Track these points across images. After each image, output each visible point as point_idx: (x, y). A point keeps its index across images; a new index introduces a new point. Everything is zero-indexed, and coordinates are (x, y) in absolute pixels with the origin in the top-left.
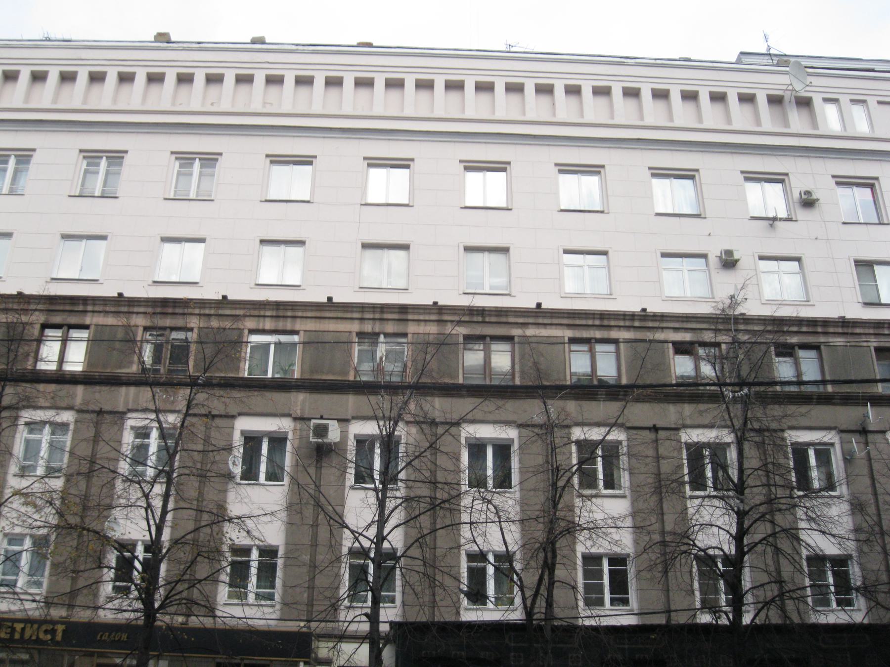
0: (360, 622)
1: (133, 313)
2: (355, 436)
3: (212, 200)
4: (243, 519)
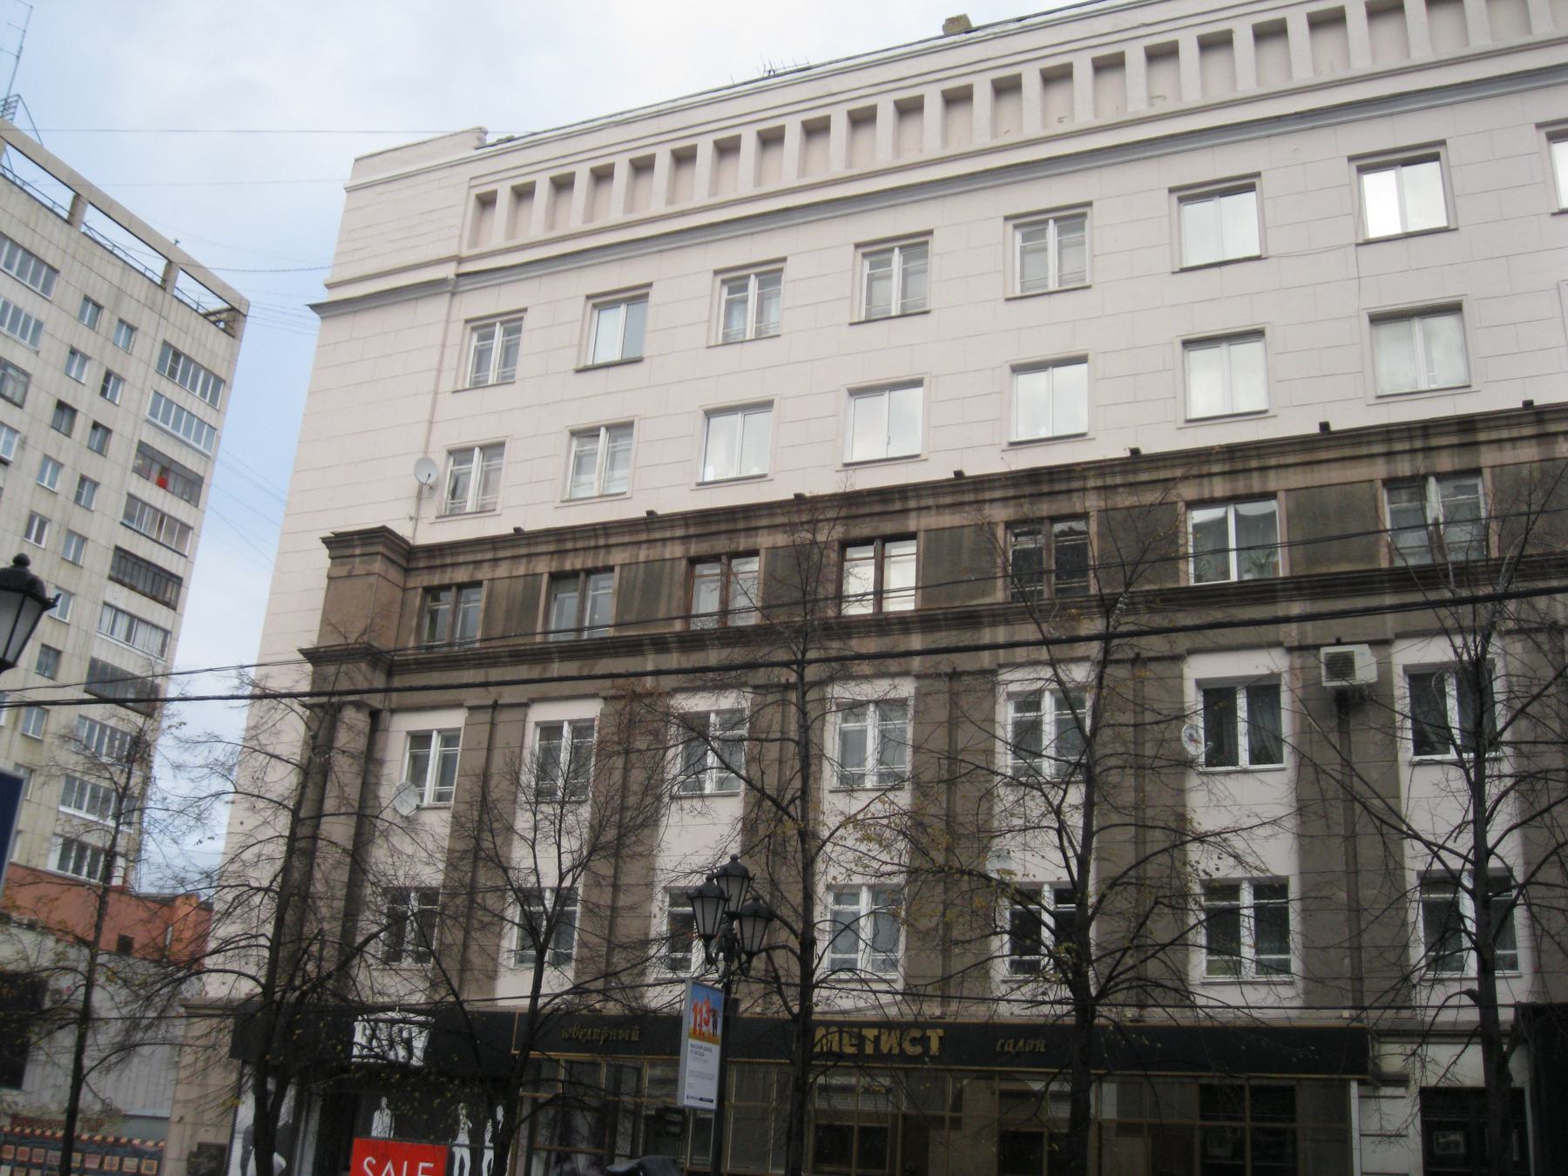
0: (1459, 1007)
1: (984, 501)
2: (1406, 669)
3: (1088, 287)
4: (1224, 836)
